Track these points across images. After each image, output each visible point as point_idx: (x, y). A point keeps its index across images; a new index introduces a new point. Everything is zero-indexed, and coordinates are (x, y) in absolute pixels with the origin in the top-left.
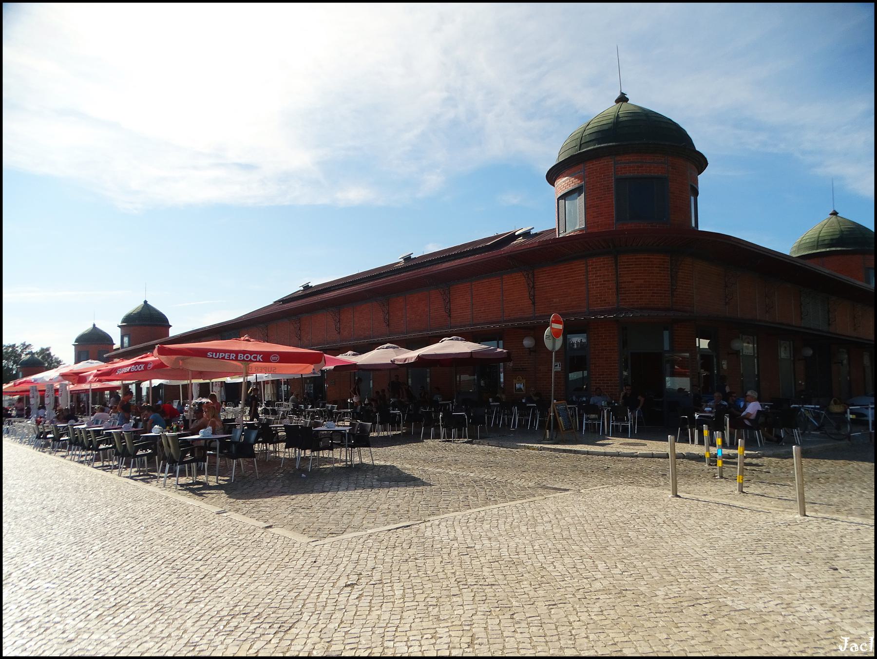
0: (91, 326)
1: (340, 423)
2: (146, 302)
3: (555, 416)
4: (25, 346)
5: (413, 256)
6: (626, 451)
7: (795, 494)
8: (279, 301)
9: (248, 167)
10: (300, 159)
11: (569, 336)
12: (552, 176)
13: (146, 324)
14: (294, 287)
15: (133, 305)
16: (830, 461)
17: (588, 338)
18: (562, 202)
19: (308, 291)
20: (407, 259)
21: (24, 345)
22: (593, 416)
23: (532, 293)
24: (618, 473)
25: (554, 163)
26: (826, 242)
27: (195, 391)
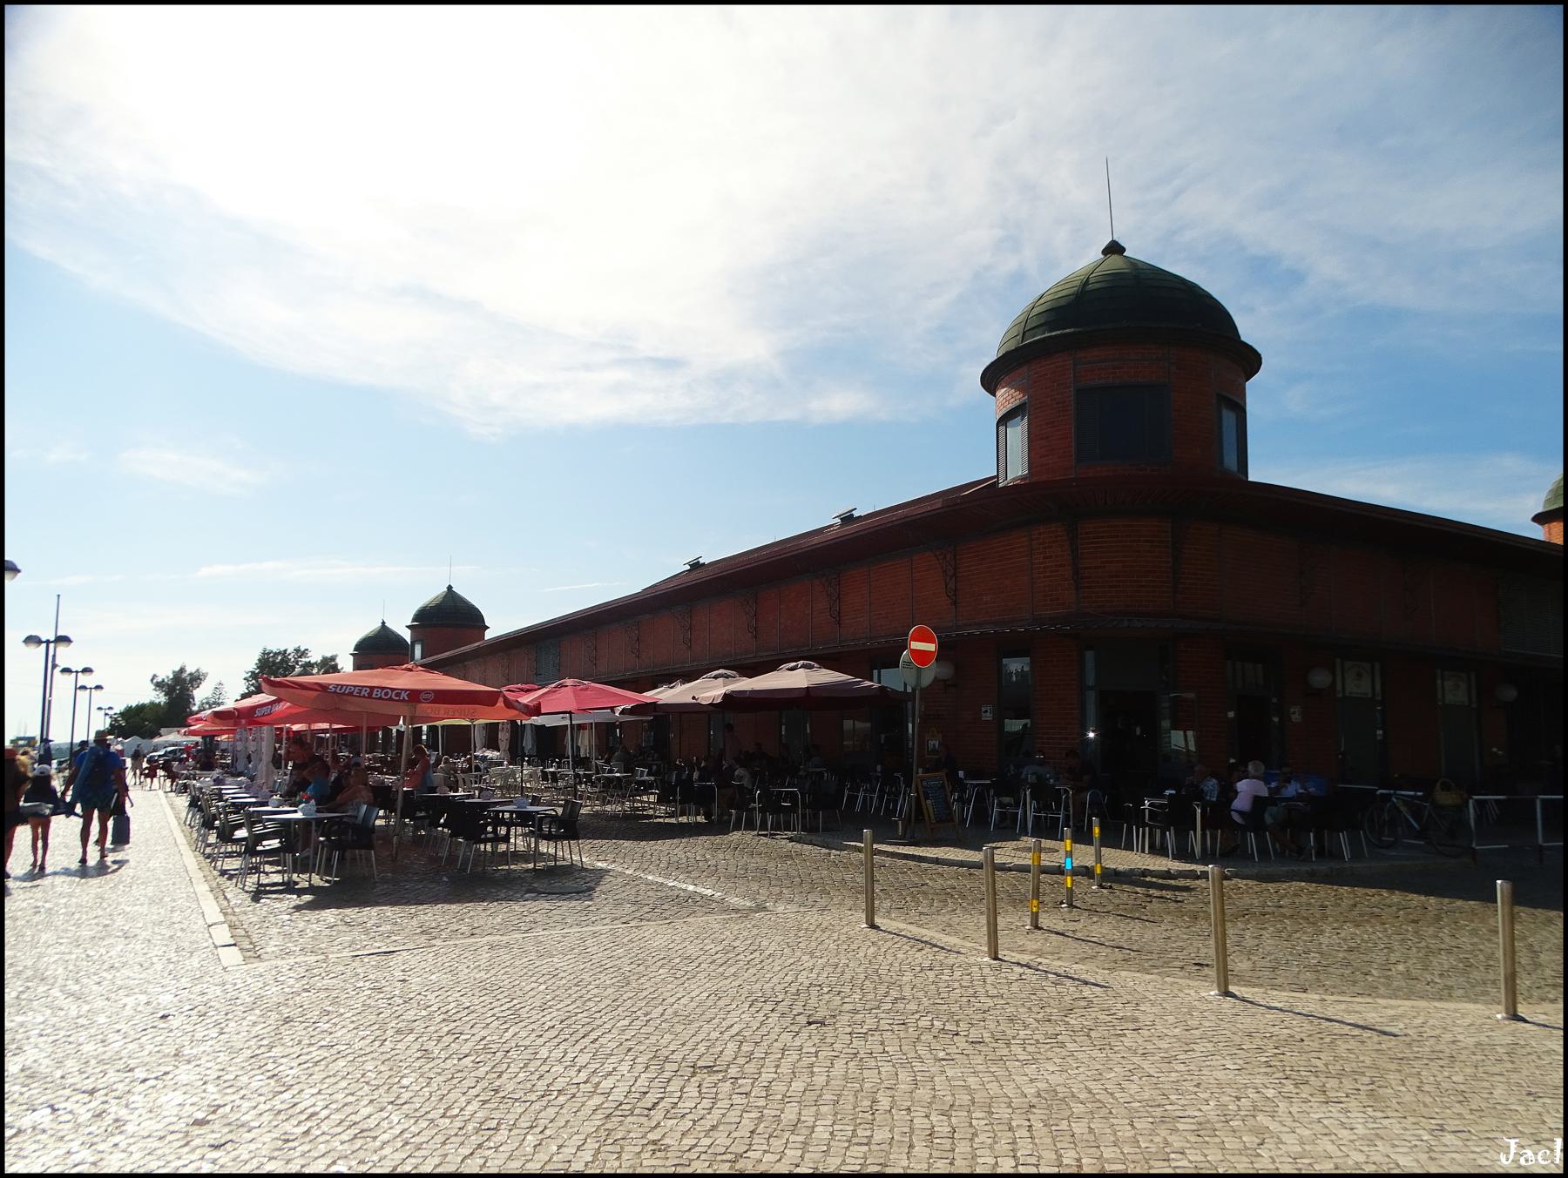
1: (645, 798)
2: (450, 588)
3: (918, 798)
5: (856, 514)
6: (1017, 861)
7: (1208, 951)
9: (670, 364)
10: (754, 348)
11: (1005, 661)
12: (991, 379)
13: (449, 621)
15: (430, 593)
16: (627, 844)
17: (1032, 664)
18: (1002, 428)
20: (848, 519)
21: (297, 650)
22: (1006, 800)
23: (951, 585)
24: (946, 894)
25: (991, 357)
27: (478, 737)
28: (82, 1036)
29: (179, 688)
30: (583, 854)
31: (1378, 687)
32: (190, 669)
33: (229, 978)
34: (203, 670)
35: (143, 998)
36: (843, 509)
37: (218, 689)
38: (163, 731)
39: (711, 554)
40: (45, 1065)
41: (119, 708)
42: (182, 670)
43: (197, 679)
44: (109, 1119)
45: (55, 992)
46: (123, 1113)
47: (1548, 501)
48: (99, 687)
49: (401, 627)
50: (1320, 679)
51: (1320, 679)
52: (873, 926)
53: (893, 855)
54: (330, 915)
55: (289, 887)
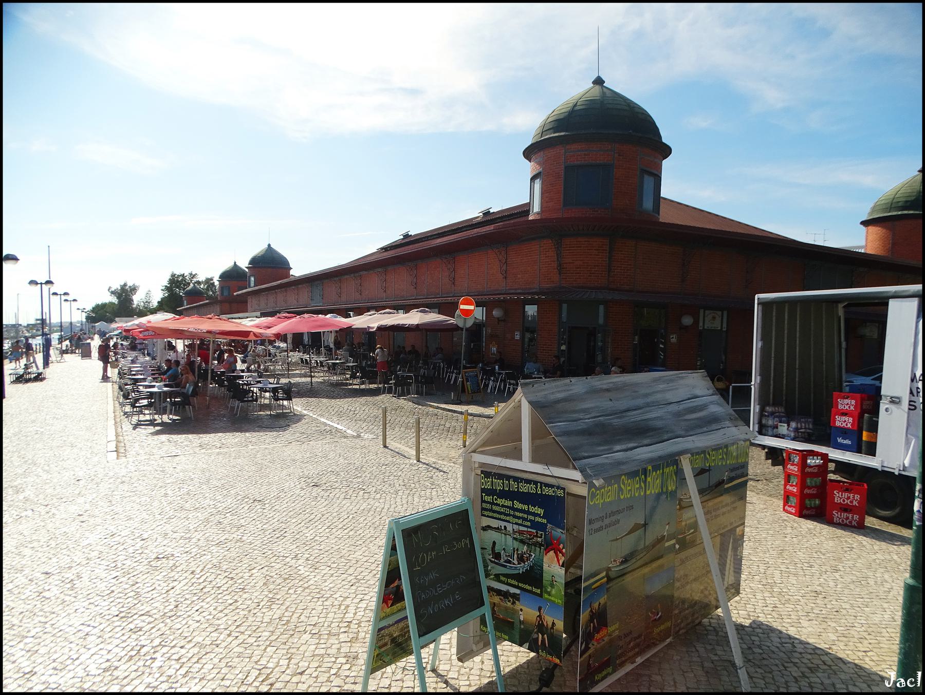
0: (231, 264)
2: (269, 245)
4: (193, 276)
5: (491, 211)
8: (382, 249)
9: (414, 92)
14: (395, 236)
15: (257, 249)
19: (408, 240)
22: (512, 382)
26: (900, 204)
28: (47, 487)
29: (125, 294)
30: (298, 405)
31: (725, 325)
32: (130, 284)
33: (108, 465)
34: (137, 284)
35: (72, 473)
36: (484, 208)
37: (148, 294)
38: (117, 319)
39: (415, 230)
40: (32, 497)
41: (89, 307)
42: (125, 285)
43: (134, 289)
44: (50, 514)
45: (39, 470)
46: (56, 512)
47: (873, 210)
48: (74, 300)
49: (244, 264)
50: (687, 321)
51: (687, 321)
52: (385, 446)
53: (438, 408)
54: (164, 437)
55: (152, 423)
